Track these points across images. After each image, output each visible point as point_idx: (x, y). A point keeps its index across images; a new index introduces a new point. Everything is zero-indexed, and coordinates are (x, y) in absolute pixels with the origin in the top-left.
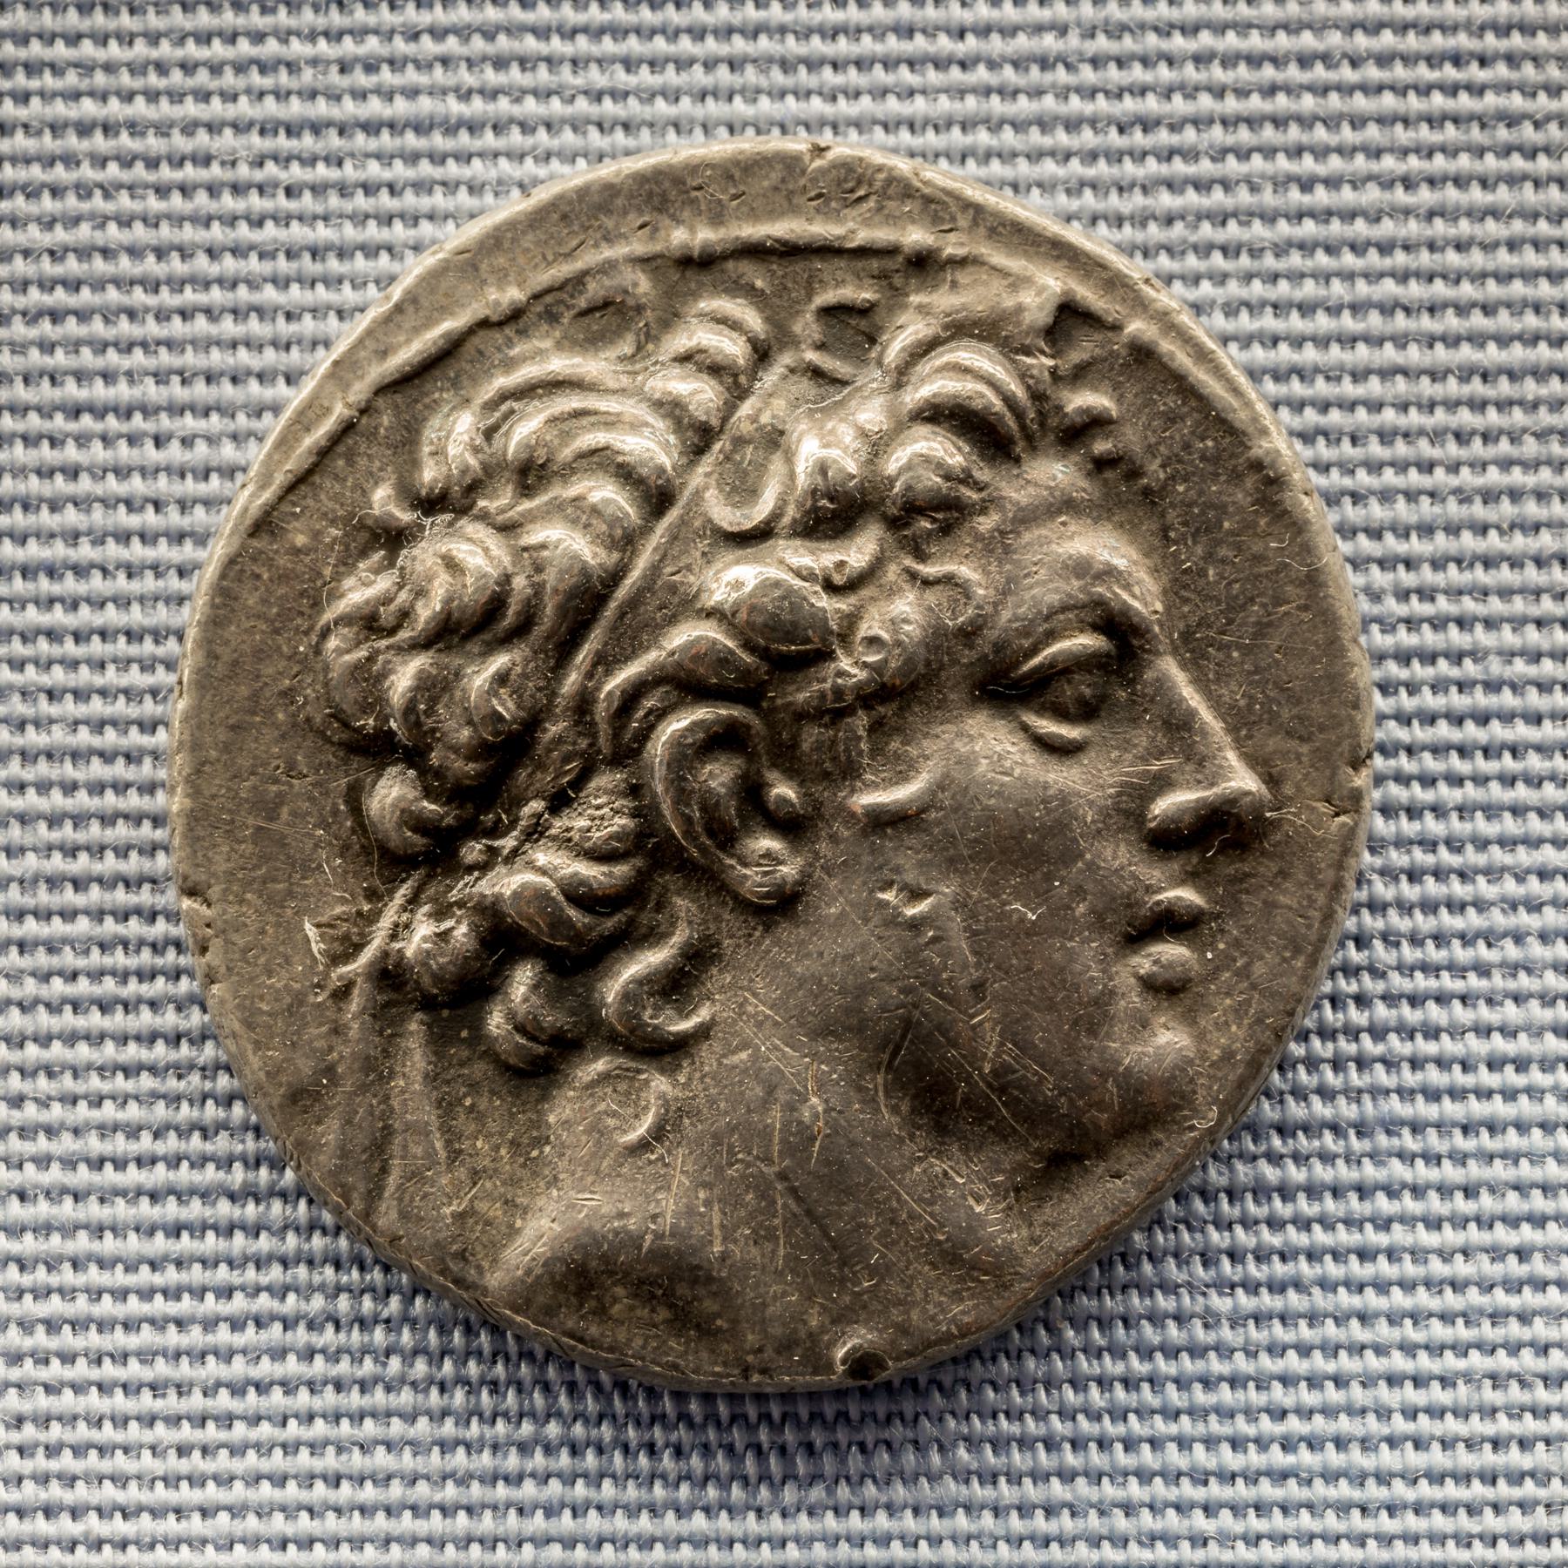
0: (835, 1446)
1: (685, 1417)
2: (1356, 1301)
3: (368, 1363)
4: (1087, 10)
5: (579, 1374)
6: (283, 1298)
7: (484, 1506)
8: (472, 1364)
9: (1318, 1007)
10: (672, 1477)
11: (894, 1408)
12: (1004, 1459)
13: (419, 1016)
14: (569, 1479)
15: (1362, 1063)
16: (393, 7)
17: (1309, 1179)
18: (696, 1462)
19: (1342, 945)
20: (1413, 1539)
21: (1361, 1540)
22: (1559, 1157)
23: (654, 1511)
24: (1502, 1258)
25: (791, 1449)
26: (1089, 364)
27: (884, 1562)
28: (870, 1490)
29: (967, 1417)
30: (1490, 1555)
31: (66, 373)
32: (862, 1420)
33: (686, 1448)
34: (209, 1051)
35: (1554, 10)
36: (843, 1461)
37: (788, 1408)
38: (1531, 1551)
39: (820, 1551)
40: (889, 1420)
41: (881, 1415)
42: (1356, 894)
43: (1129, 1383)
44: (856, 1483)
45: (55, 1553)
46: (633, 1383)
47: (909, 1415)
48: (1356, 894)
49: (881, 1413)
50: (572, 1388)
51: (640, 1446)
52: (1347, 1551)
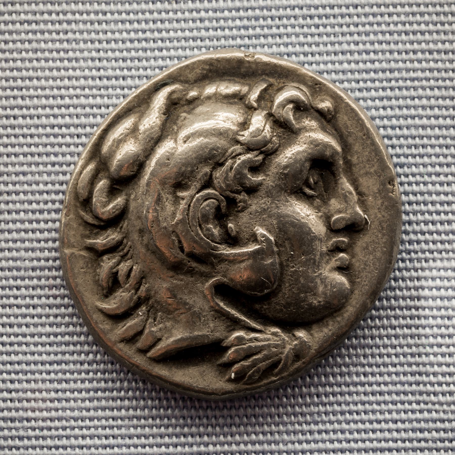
5: (177, 396)
7: (166, 435)
9: (390, 282)
10: (214, 425)
11: (233, 405)
12: (328, 418)
14: (167, 427)
16: (177, 3)
18: (205, 421)
19: (398, 262)
20: (136, 446)
21: (129, 447)
22: (453, 14)
23: (185, 436)
24: (415, 357)
26: (196, 99)
27: (136, 453)
28: (266, 428)
29: (278, 408)
30: (143, 451)
31: (81, 115)
32: (216, 408)
33: (202, 417)
37: (208, 404)
38: (116, 450)
39: (171, 449)
40: (231, 408)
41: (229, 407)
42: (401, 247)
43: (342, 394)
45: (61, 450)
48: (401, 247)
49: (252, 405)
50: (175, 400)
52: (124, 450)
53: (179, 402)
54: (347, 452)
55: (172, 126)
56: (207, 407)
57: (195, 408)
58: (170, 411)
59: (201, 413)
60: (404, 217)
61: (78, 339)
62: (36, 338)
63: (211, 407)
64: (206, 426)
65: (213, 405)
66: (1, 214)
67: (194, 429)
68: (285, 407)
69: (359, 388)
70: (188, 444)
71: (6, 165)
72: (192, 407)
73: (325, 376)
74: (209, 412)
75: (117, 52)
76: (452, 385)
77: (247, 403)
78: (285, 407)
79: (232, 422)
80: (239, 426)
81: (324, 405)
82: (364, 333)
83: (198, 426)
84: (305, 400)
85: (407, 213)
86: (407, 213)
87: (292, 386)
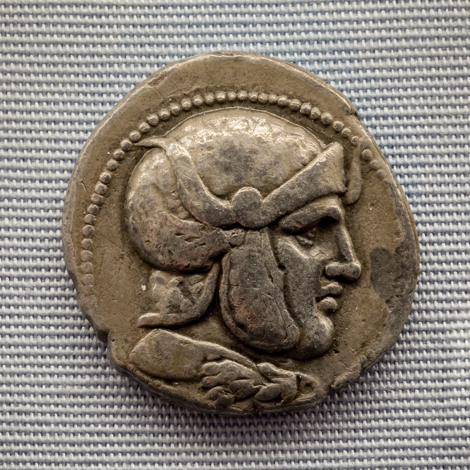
0: (258, 432)
1: (220, 424)
2: (8, 389)
3: (116, 408)
4: (435, 3)
6: (105, 388)
8: (164, 409)
13: (336, 308)
15: (427, 311)
17: (427, 347)
18: (215, 438)
25: (252, 433)
34: (76, 311)
35: (467, 2)
36: (244, 438)
40: (266, 424)
44: (281, 443)
46: (204, 414)
47: (280, 423)
50: (185, 416)
51: (247, 432)
53: (181, 418)
54: (457, 467)
55: (184, 131)
56: (250, 424)
57: (197, 424)
58: (179, 428)
59: (219, 429)
60: (421, 247)
61: (87, 352)
62: (52, 349)
63: (237, 424)
64: (224, 443)
65: (239, 422)
66: (1, 201)
67: (229, 447)
68: (305, 423)
69: (390, 404)
70: (206, 462)
71: (6, 149)
72: (194, 424)
73: (354, 393)
74: (228, 429)
75: (87, 37)
76: (467, 166)
77: (275, 421)
78: (305, 423)
79: (284, 439)
80: (274, 443)
81: (354, 421)
82: (339, 408)
83: (217, 444)
84: (327, 417)
85: (424, 244)
86: (424, 244)
87: (336, 402)
